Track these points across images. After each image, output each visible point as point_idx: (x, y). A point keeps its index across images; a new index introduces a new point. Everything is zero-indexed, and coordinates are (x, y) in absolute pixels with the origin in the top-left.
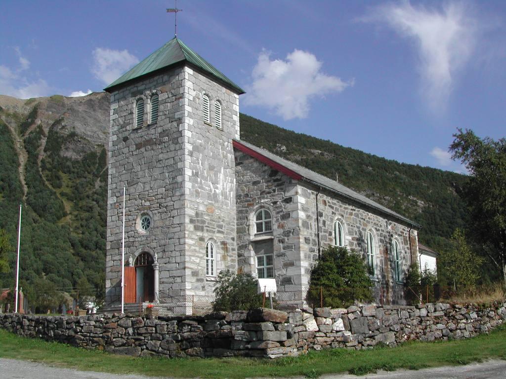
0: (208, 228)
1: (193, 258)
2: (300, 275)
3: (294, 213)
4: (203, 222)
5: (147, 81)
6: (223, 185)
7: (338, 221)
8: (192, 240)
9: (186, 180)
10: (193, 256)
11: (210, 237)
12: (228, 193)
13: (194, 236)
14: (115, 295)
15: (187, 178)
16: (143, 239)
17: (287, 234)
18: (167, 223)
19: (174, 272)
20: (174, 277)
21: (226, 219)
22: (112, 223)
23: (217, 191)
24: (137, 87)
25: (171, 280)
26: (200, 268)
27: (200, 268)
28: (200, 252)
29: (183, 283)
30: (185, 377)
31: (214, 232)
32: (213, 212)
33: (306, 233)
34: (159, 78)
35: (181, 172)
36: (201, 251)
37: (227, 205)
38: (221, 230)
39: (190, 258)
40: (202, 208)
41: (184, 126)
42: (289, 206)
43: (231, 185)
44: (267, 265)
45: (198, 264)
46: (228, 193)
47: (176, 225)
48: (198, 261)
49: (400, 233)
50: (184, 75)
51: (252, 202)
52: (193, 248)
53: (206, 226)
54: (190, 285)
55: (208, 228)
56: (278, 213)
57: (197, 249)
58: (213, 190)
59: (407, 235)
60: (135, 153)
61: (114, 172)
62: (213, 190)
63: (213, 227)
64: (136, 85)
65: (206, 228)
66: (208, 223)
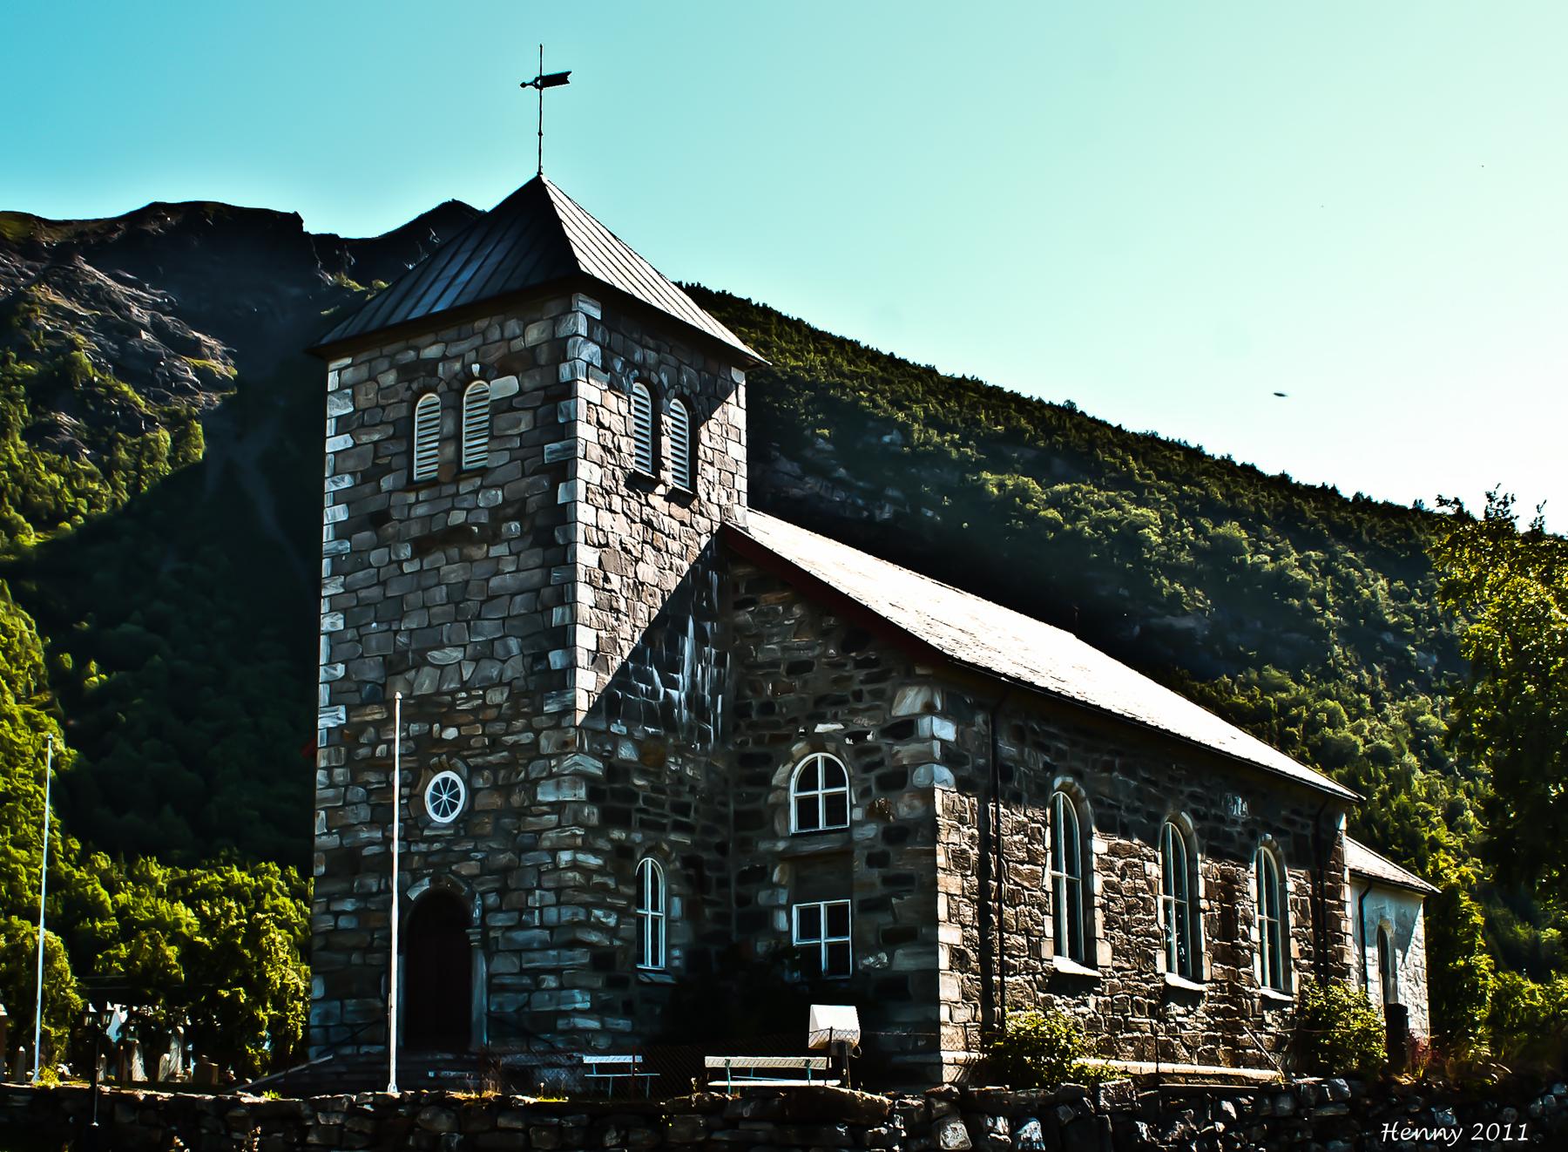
0: (645, 817)
1: (598, 913)
2: (936, 971)
3: (922, 770)
4: (631, 795)
5: (451, 333)
6: (693, 674)
7: (1062, 794)
8: (596, 857)
9: (580, 664)
10: (599, 907)
11: (650, 844)
12: (708, 698)
13: (602, 844)
14: (342, 1024)
15: (583, 658)
16: (437, 846)
17: (897, 834)
18: (516, 799)
19: (536, 955)
20: (536, 973)
21: (702, 785)
22: (330, 792)
23: (674, 693)
24: (417, 349)
25: (526, 981)
26: (617, 943)
27: (617, 943)
28: (616, 893)
29: (564, 993)
30: (1460, 504)
31: (662, 828)
32: (662, 762)
33: (954, 838)
34: (489, 326)
35: (564, 638)
36: (623, 889)
37: (704, 738)
38: (684, 819)
39: (589, 914)
40: (626, 752)
41: (573, 492)
42: (905, 751)
43: (719, 673)
44: (828, 785)
45: (612, 932)
46: (708, 698)
47: (545, 808)
48: (612, 921)
49: (1283, 827)
50: (575, 324)
51: (784, 731)
52: (597, 879)
53: (640, 810)
54: (588, 998)
55: (645, 817)
56: (869, 768)
57: (611, 883)
58: (662, 690)
59: (1309, 832)
60: (407, 568)
61: (340, 625)
62: (662, 690)
63: (659, 811)
64: (412, 342)
65: (639, 816)
66: (646, 800)
